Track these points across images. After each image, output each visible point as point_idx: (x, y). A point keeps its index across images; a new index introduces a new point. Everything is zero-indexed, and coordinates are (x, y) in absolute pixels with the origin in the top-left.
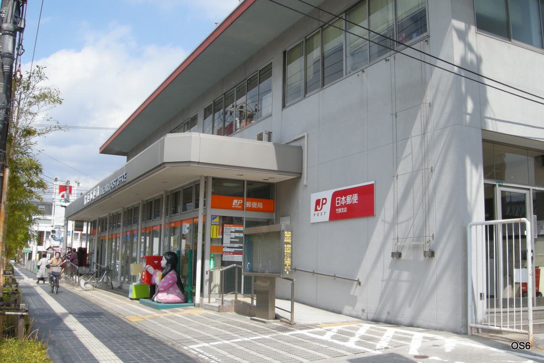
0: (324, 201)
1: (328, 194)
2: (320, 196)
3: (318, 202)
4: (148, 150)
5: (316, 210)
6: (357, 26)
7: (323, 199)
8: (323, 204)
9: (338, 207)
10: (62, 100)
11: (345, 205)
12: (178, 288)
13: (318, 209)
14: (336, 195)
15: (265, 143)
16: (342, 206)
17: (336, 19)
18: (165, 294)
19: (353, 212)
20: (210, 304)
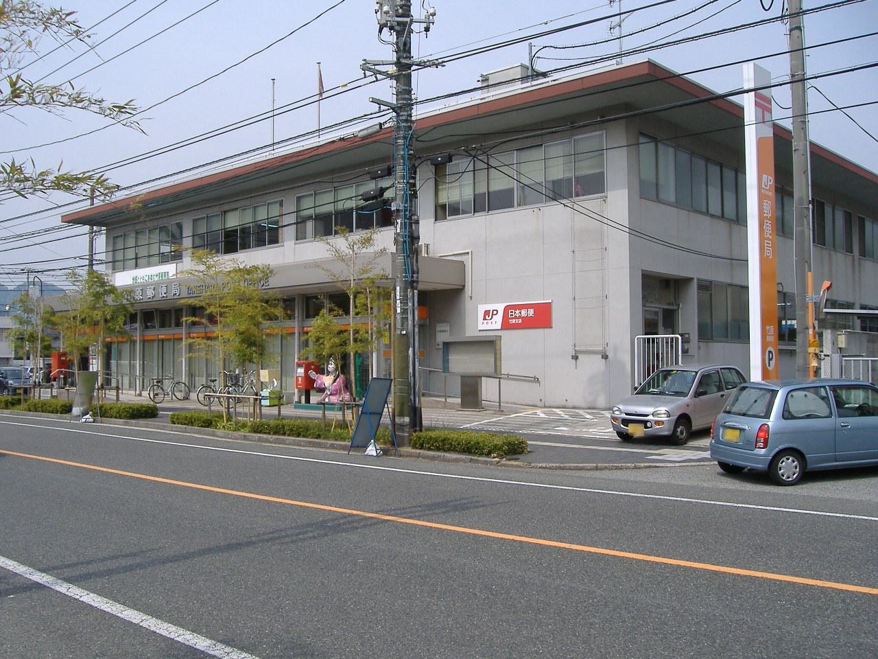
0: (495, 312)
1: (500, 308)
2: (490, 307)
3: (487, 313)
4: (536, 300)
5: (485, 319)
6: (734, 195)
7: (493, 311)
8: (493, 314)
9: (512, 318)
10: (348, 246)
11: (520, 317)
12: (773, 176)
13: (487, 318)
14: (507, 309)
15: (46, 9)
16: (516, 318)
17: (11, 195)
18: (384, 187)
19: (528, 324)
20: (95, 206)
